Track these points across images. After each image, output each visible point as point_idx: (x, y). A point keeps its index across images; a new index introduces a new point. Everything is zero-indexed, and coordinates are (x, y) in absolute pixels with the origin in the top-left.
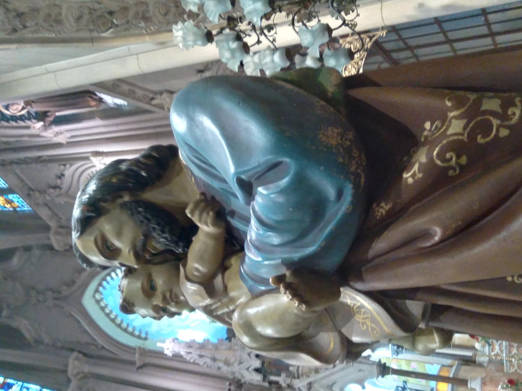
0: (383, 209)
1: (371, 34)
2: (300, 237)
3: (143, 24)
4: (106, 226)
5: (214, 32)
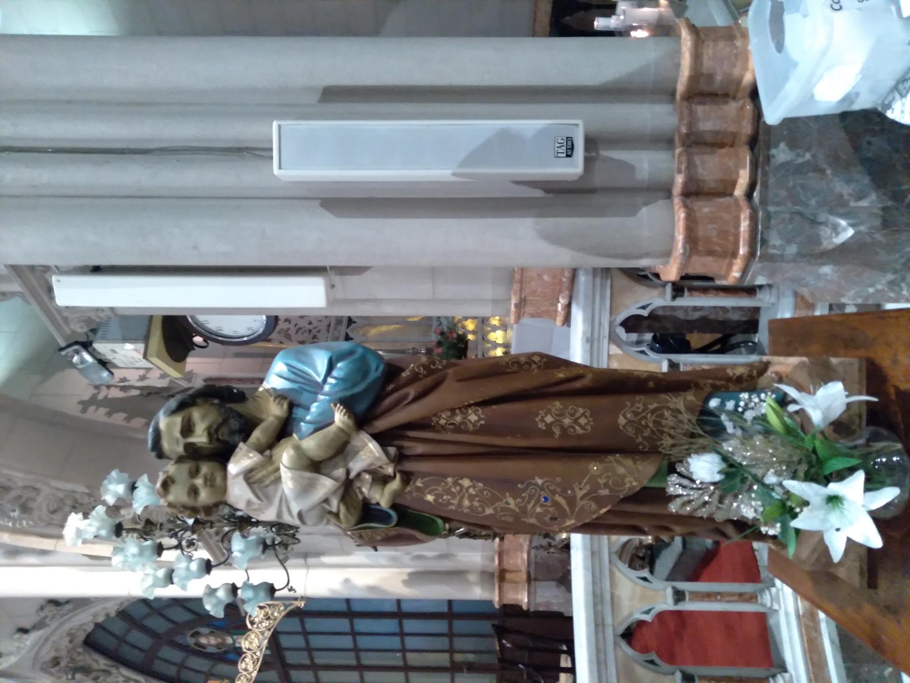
0: (391, 387)
1: (288, 603)
2: (354, 385)
3: (16, 514)
4: (196, 414)
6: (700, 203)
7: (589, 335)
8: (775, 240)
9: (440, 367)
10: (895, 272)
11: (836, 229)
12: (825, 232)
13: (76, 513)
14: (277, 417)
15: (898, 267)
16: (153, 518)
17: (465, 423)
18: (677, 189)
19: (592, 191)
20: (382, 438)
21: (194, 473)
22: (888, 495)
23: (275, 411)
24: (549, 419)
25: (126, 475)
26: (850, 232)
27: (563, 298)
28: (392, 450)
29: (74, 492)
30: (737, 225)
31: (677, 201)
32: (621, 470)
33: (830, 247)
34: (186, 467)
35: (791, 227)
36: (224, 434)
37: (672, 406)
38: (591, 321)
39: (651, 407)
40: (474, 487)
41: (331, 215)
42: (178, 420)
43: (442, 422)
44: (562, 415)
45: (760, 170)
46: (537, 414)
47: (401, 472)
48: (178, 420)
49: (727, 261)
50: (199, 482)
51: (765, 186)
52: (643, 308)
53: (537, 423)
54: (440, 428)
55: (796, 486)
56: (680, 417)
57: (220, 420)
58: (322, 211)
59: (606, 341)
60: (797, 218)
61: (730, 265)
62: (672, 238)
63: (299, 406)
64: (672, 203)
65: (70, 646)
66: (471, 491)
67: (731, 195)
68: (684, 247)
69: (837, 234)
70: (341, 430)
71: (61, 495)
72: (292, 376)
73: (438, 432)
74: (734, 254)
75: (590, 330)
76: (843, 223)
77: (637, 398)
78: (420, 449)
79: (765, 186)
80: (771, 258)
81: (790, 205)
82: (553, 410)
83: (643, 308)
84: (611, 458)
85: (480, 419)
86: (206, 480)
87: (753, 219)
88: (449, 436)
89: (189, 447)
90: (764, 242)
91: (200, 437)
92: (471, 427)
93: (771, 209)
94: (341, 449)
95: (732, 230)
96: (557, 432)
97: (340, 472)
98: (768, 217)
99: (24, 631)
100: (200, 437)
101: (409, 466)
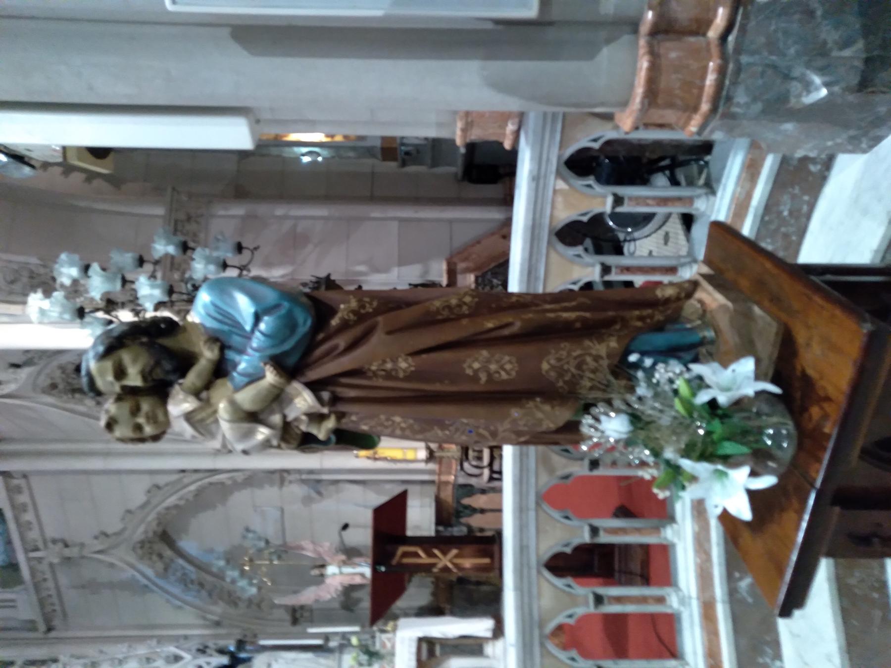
0: (321, 336)
2: (283, 341)
4: (126, 356)
5: (87, 310)
6: (668, 44)
7: (535, 173)
8: (741, 97)
9: (371, 310)
10: (859, 128)
11: (808, 87)
12: (795, 87)
13: (35, 292)
14: (209, 360)
15: (863, 124)
16: (112, 297)
17: (396, 370)
18: (645, 28)
19: (551, 24)
20: (314, 387)
21: (135, 411)
22: (766, 481)
23: (208, 354)
24: (476, 365)
25: (76, 257)
26: (824, 92)
27: (513, 124)
28: (326, 395)
29: (28, 264)
30: (703, 77)
31: (642, 42)
32: (539, 415)
33: (798, 107)
34: (126, 406)
35: (760, 82)
36: (159, 374)
37: (594, 352)
38: (539, 160)
39: (575, 354)
40: (405, 422)
41: (245, 53)
42: (109, 364)
43: (374, 368)
44: (488, 361)
45: (741, 11)
46: (464, 362)
47: (336, 413)
48: (109, 364)
49: (687, 114)
50: (141, 420)
51: (743, 30)
52: (595, 140)
53: (464, 369)
54: (370, 374)
55: (686, 464)
56: (601, 362)
57: (152, 362)
58: (235, 48)
59: (552, 177)
60: (770, 72)
61: (689, 119)
62: (632, 86)
63: (230, 347)
64: (637, 43)
65: (64, 376)
66: (403, 425)
67: (704, 34)
68: (642, 103)
69: (809, 92)
70: (273, 386)
71: (16, 267)
72: (220, 317)
73: (370, 378)
74: (696, 109)
75: (537, 167)
76: (817, 80)
77: (562, 345)
78: (352, 393)
79: (743, 30)
80: (733, 116)
81: (765, 54)
82: (481, 358)
83: (595, 140)
84: (531, 404)
85: (410, 366)
86: (148, 418)
87: (722, 72)
88: (380, 382)
89: (124, 388)
90: (729, 99)
91: (134, 379)
92: (401, 375)
93: (745, 59)
94: (277, 398)
95: (698, 82)
96: (483, 377)
97: (276, 419)
98: (739, 70)
99: (16, 366)
100: (134, 379)
101: (342, 408)
